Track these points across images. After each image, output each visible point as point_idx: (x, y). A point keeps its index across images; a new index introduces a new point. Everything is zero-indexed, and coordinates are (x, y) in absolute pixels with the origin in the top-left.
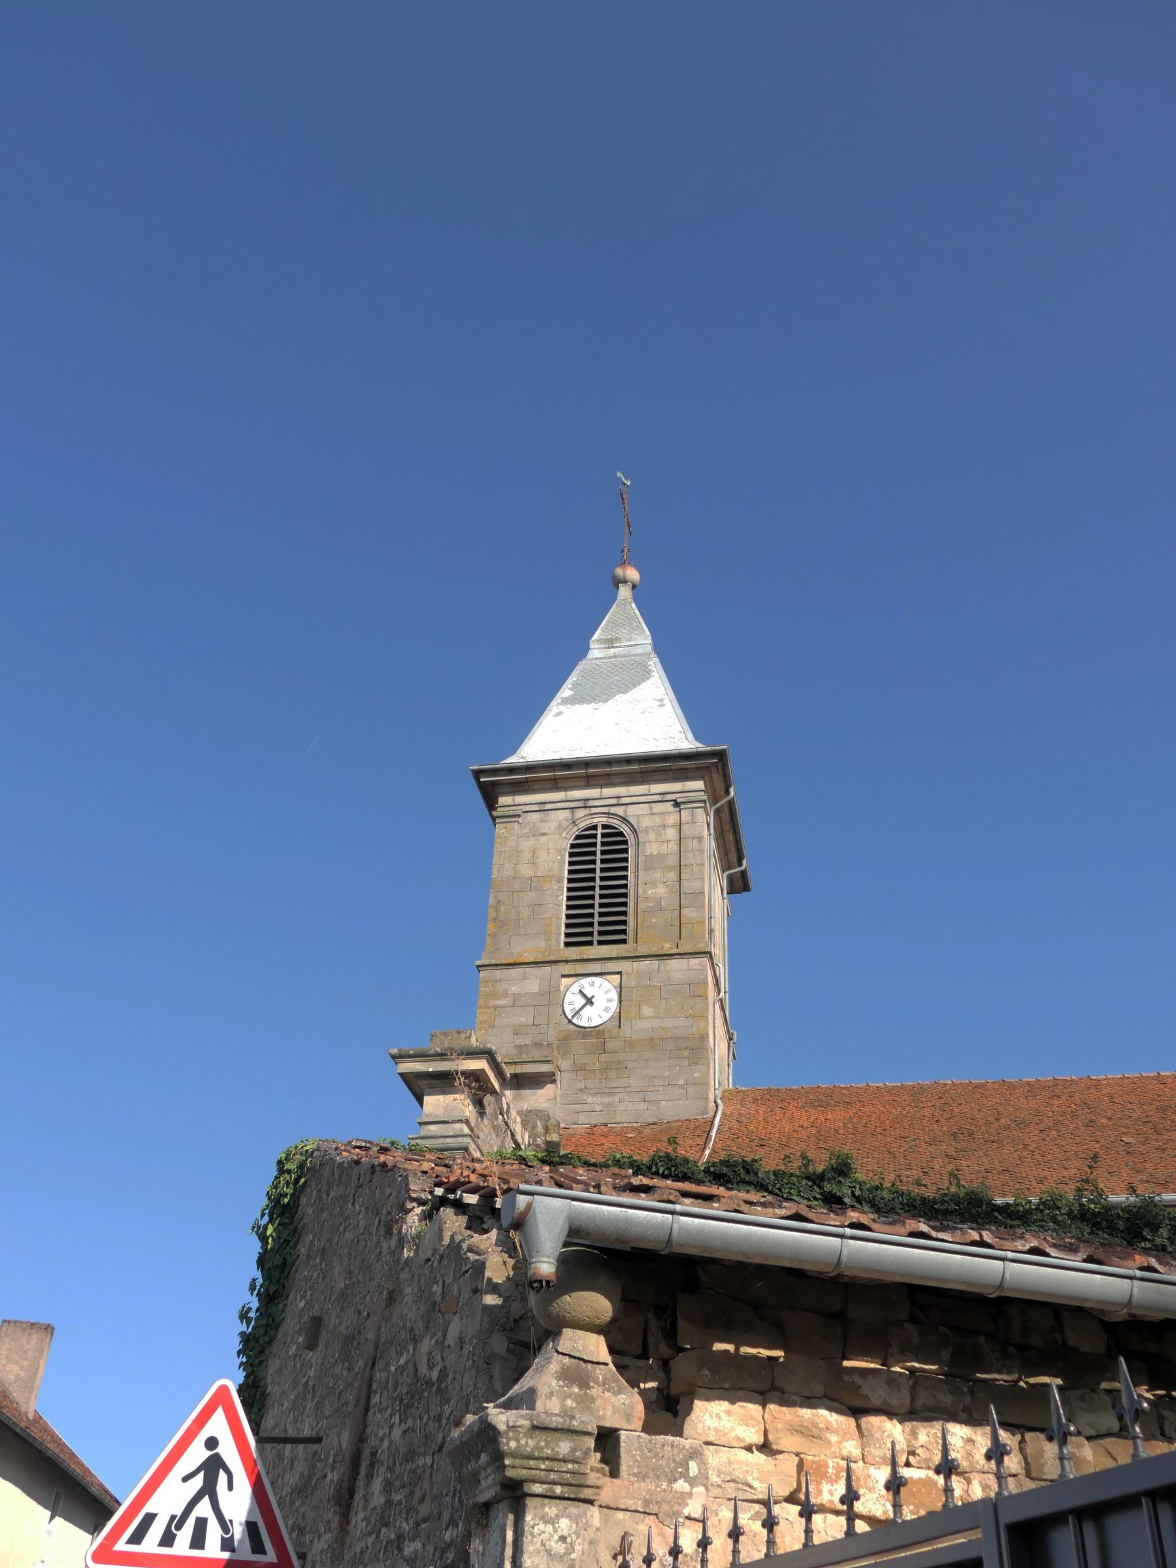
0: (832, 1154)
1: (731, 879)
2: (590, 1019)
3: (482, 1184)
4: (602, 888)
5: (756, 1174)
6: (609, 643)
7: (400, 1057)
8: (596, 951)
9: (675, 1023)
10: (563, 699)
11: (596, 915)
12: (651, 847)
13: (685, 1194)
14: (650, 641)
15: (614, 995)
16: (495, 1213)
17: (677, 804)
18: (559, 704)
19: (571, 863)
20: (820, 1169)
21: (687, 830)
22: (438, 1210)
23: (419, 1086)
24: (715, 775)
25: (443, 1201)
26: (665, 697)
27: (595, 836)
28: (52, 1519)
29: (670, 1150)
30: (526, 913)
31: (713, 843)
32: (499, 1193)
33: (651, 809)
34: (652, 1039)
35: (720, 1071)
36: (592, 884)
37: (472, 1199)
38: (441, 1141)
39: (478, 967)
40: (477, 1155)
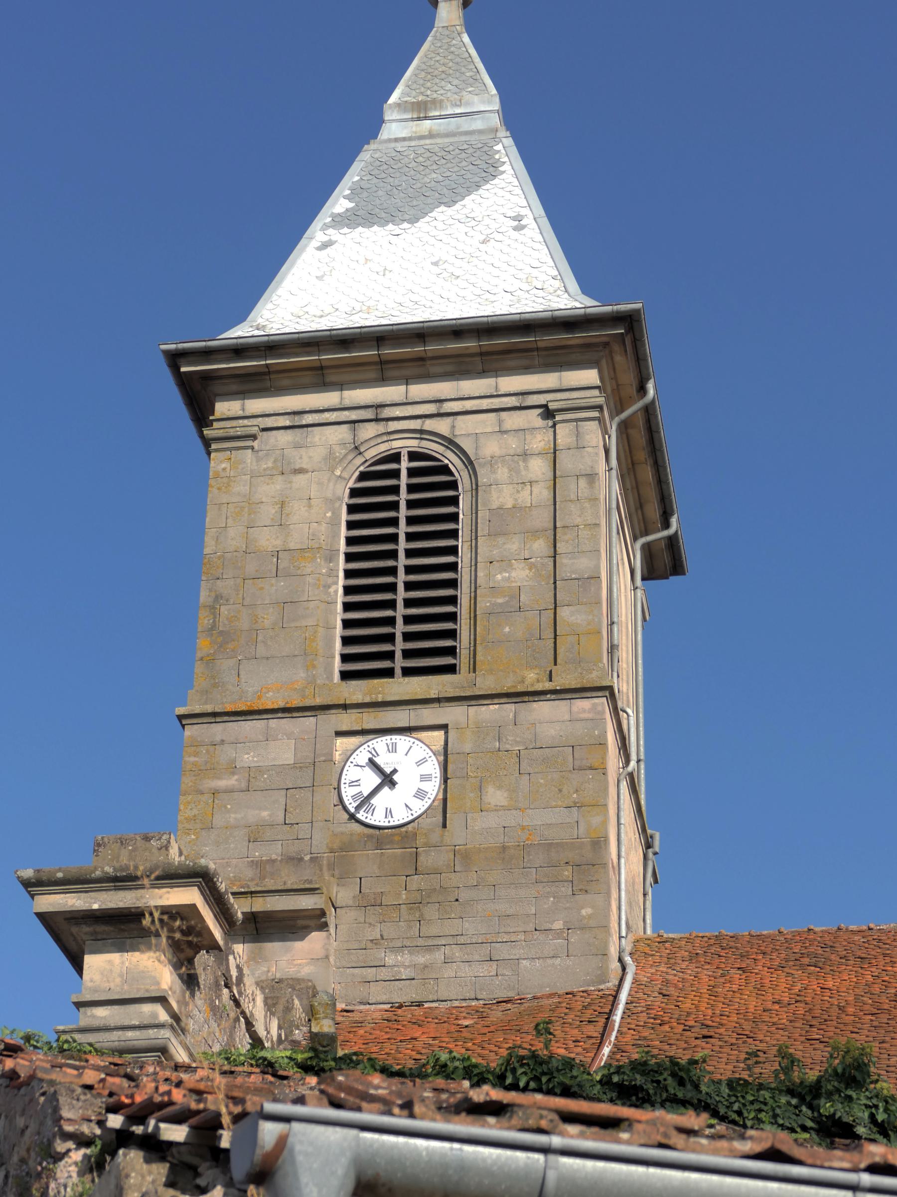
0: (836, 1048)
1: (648, 552)
2: (389, 812)
3: (194, 1106)
4: (409, 570)
5: (697, 1087)
6: (420, 110)
7: (39, 883)
8: (400, 687)
9: (548, 819)
10: (334, 217)
11: (400, 621)
12: (501, 493)
13: (569, 1118)
14: (496, 106)
15: (433, 768)
16: (220, 1157)
17: (548, 413)
18: (326, 227)
19: (351, 525)
20: (812, 1076)
21: (566, 462)
22: (114, 1154)
23: (74, 937)
24: (619, 359)
25: (123, 1138)
26: (526, 211)
27: (396, 474)
28: (395, 771)
29: (539, 1046)
30: (269, 618)
31: (616, 486)
32: (226, 1120)
33: (500, 422)
34: (504, 848)
35: (630, 904)
36: (390, 563)
37: (176, 1133)
38: (116, 1035)
39: (180, 718)
40: (182, 1056)
